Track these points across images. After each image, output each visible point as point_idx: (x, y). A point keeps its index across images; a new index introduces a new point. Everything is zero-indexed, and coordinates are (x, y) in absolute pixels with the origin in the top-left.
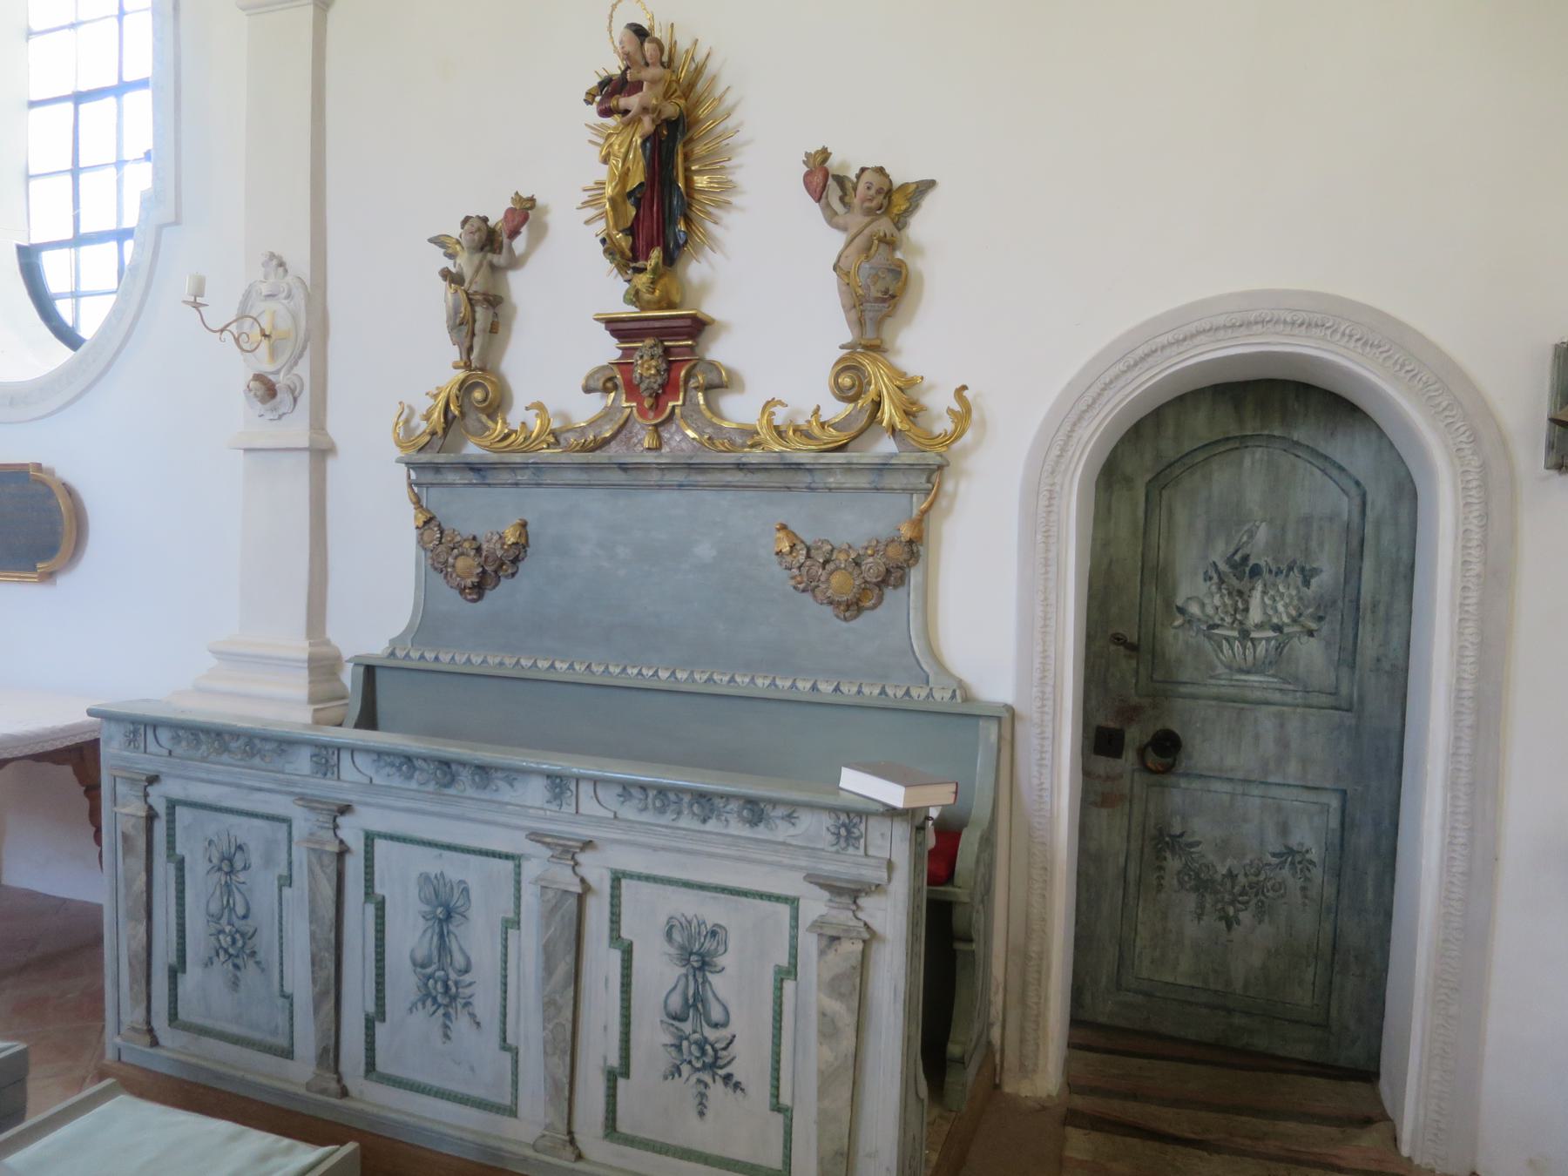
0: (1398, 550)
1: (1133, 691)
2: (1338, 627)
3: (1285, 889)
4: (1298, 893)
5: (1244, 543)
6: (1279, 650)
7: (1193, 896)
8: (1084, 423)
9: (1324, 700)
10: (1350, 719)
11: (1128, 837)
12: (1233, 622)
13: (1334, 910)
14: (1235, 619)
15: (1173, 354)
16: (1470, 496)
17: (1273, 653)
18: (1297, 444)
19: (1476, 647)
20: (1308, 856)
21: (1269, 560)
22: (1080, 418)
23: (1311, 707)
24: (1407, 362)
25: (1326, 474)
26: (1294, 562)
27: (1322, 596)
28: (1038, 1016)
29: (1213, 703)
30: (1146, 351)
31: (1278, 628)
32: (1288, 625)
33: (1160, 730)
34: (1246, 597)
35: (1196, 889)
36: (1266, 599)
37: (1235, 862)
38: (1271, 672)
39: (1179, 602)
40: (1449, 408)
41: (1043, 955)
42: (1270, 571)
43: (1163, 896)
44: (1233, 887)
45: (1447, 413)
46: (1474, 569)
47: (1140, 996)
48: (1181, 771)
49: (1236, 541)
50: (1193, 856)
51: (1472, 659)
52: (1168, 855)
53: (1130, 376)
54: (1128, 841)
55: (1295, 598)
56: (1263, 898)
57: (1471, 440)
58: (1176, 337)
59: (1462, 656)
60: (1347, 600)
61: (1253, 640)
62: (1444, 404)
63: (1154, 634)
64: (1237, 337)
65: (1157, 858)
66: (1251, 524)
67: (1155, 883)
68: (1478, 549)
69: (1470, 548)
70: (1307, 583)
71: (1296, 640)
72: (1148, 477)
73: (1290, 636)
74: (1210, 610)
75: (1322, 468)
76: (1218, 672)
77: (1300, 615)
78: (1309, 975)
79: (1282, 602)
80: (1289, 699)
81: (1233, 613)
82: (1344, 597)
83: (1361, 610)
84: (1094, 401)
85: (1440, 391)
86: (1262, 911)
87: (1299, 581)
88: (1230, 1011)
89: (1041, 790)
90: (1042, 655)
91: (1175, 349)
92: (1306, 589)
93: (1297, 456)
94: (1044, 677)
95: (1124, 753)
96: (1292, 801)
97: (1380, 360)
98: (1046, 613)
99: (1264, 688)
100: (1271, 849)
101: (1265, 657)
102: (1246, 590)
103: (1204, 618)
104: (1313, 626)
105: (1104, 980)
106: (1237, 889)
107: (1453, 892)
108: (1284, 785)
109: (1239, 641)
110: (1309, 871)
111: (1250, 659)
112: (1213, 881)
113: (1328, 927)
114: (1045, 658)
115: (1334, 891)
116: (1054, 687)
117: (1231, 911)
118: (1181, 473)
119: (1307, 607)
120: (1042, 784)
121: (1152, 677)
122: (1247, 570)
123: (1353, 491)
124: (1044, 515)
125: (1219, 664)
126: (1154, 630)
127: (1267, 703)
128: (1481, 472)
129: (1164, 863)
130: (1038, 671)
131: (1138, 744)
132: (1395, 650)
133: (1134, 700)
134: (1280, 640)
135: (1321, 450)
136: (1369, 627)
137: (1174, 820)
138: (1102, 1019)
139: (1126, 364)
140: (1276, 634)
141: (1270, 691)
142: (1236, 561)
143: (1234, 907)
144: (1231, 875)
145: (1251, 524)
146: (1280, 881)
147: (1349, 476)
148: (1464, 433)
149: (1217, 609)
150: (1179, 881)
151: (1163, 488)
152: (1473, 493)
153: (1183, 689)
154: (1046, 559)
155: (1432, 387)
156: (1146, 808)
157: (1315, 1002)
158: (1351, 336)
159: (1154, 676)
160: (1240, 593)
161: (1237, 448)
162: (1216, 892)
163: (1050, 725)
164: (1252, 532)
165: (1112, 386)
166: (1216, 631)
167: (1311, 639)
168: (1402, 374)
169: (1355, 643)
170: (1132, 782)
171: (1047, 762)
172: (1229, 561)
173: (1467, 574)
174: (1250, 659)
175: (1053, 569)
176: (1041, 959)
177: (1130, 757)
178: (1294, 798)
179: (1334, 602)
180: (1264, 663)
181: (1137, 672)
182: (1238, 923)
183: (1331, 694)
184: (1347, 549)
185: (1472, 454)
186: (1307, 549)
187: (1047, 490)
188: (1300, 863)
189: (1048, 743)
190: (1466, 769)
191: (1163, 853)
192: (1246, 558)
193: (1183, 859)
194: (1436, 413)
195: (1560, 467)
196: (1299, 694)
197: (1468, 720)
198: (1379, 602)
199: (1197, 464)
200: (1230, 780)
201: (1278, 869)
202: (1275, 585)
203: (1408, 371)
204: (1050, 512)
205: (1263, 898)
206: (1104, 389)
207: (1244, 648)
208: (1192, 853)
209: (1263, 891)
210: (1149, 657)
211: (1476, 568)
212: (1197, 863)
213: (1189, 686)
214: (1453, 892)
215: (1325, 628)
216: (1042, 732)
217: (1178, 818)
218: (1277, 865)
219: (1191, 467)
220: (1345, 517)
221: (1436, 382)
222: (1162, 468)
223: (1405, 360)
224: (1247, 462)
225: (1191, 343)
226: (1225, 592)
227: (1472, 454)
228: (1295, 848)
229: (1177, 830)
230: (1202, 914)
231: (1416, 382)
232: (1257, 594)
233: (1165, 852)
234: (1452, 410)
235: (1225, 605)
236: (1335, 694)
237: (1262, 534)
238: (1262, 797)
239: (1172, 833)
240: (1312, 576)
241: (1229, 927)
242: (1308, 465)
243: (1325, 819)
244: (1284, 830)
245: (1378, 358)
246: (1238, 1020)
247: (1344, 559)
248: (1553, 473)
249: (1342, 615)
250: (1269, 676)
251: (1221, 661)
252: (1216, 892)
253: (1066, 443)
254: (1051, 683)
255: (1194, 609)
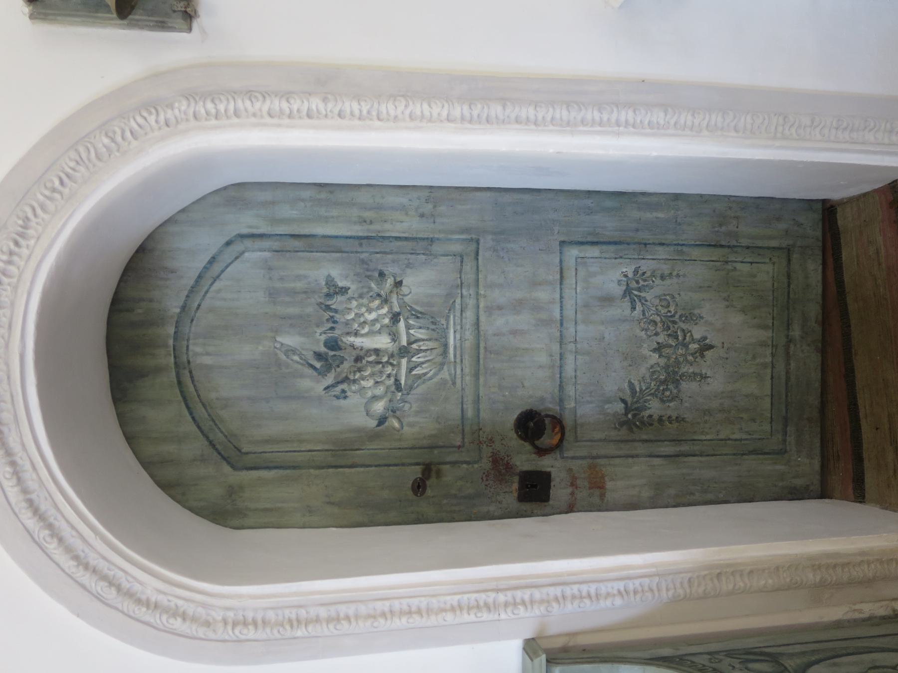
0: (303, 200)
1: (476, 466)
2: (390, 256)
3: (665, 295)
4: (668, 282)
5: (301, 358)
6: (419, 315)
7: (684, 385)
8: (137, 587)
9: (469, 266)
10: (487, 241)
11: (632, 457)
12: (392, 364)
13: (680, 248)
14: (387, 362)
15: (34, 476)
16: (226, 111)
17: (421, 321)
18: (184, 308)
19: (411, 103)
20: (630, 275)
21: (319, 331)
22: (129, 594)
23: (477, 280)
24: (49, 185)
25: (218, 277)
26: (320, 304)
27: (357, 274)
28: (881, 562)
29: (482, 380)
30: (30, 514)
31: (395, 318)
32: (391, 308)
33: (517, 433)
34: (362, 353)
35: (677, 383)
36: (363, 332)
37: (645, 345)
38: (443, 322)
39: (372, 423)
40: (110, 134)
41: (815, 563)
42: (332, 329)
43: (688, 416)
44: (671, 346)
45: (119, 139)
46: (317, 106)
47: (788, 428)
48: (558, 408)
49: (300, 367)
50: (644, 388)
51: (425, 106)
52: (646, 413)
53: (66, 532)
54: (637, 456)
55: (361, 301)
56: (677, 316)
57: (153, 111)
58: (8, 476)
59: (423, 117)
60: (359, 250)
61: (410, 343)
62: (106, 141)
63: (411, 448)
64: (12, 396)
65: (651, 425)
66: (278, 352)
67: (675, 425)
68: (292, 101)
69: (291, 111)
70: (344, 291)
71: (407, 299)
72: (227, 469)
73: (403, 305)
74: (380, 390)
75: (212, 280)
76: (448, 377)
77: (379, 295)
78: (745, 268)
79: (366, 314)
80: (471, 302)
81: (381, 366)
82: (357, 252)
83: (370, 235)
84: (104, 578)
85: (89, 145)
86: (690, 317)
87: (340, 298)
88: (790, 341)
89: (627, 592)
90: (458, 612)
91: (29, 476)
92: (349, 291)
93: (198, 308)
94: (487, 606)
95: (543, 470)
96: (576, 293)
97: (46, 217)
98: (402, 613)
99: (462, 328)
100: (628, 312)
101: (428, 328)
102: (354, 353)
103: (389, 395)
104: (390, 281)
105: (778, 467)
106: (672, 342)
107: (685, 123)
108: (561, 302)
109: (412, 357)
110: (644, 273)
111: (431, 345)
112: (667, 367)
113: (696, 253)
114: (461, 608)
115: (660, 248)
116: (498, 590)
117: (694, 346)
118: (222, 432)
119: (370, 289)
120: (619, 592)
121: (459, 447)
122: (331, 353)
123: (238, 247)
124: (268, 630)
125: (439, 377)
126: (406, 448)
127: (477, 324)
128: (194, 99)
129: (656, 417)
130: (479, 615)
131: (534, 456)
132: (410, 200)
133: (486, 464)
134: (407, 314)
135: (192, 282)
136: (387, 226)
137: (609, 411)
138: (817, 464)
139: (48, 539)
140: (402, 319)
141: (464, 321)
142: (321, 366)
143: (690, 343)
144: (659, 349)
145: (278, 352)
146: (658, 301)
147: (220, 252)
148: (145, 119)
149: (377, 382)
150: (670, 401)
151: (240, 451)
152: (222, 107)
153: (470, 413)
154: (329, 620)
155: (84, 155)
156: (600, 440)
157: (767, 260)
158: (11, 253)
159: (458, 443)
160: (358, 359)
161: (190, 372)
162: (678, 363)
163: (545, 590)
164: (287, 351)
165: (82, 555)
166: (403, 382)
167: (404, 283)
168: (66, 191)
169: (406, 239)
170: (573, 458)
171: (593, 588)
172: (322, 373)
173: (324, 112)
174: (431, 345)
175: (343, 609)
176: (819, 567)
177: (547, 463)
178: (574, 292)
179: (363, 262)
180: (433, 330)
181: (453, 463)
182: (705, 338)
183: (462, 262)
184: (303, 251)
185: (173, 109)
186: (305, 292)
187: (233, 629)
188: (637, 282)
189: (568, 591)
190: (551, 110)
191: (645, 418)
192: (319, 356)
193: (649, 398)
194: (118, 150)
195: (188, 16)
196: (465, 292)
197: (496, 109)
198: (360, 217)
199: (209, 415)
200: (562, 357)
201: (648, 303)
202: (347, 323)
203: (62, 183)
204: (264, 622)
205: (677, 316)
206: (86, 567)
207: (419, 351)
208: (641, 390)
209: (671, 316)
210: (436, 451)
211: (316, 103)
212: (651, 383)
213: (465, 406)
214: (685, 123)
215: (390, 269)
216: (556, 599)
217: (606, 407)
218: (643, 304)
219: (213, 421)
220: (267, 254)
221: (76, 150)
222: (215, 454)
223: (46, 187)
224: (208, 360)
225: (20, 455)
226: (358, 375)
227: (173, 109)
228: (624, 288)
229: (620, 407)
230: (701, 375)
231: (76, 174)
232: (358, 341)
233: (643, 417)
234: (114, 132)
235: (372, 375)
236: (462, 257)
237: (290, 340)
238: (576, 323)
239: (623, 411)
240: (336, 286)
241: (710, 347)
242: (209, 295)
243: (592, 260)
244: (607, 300)
245: (43, 220)
246: (796, 332)
247: (315, 254)
248: (195, 25)
249: (377, 253)
250: (448, 324)
251: (436, 374)
252: (678, 363)
253: (166, 610)
254: (493, 595)
255: (379, 407)
